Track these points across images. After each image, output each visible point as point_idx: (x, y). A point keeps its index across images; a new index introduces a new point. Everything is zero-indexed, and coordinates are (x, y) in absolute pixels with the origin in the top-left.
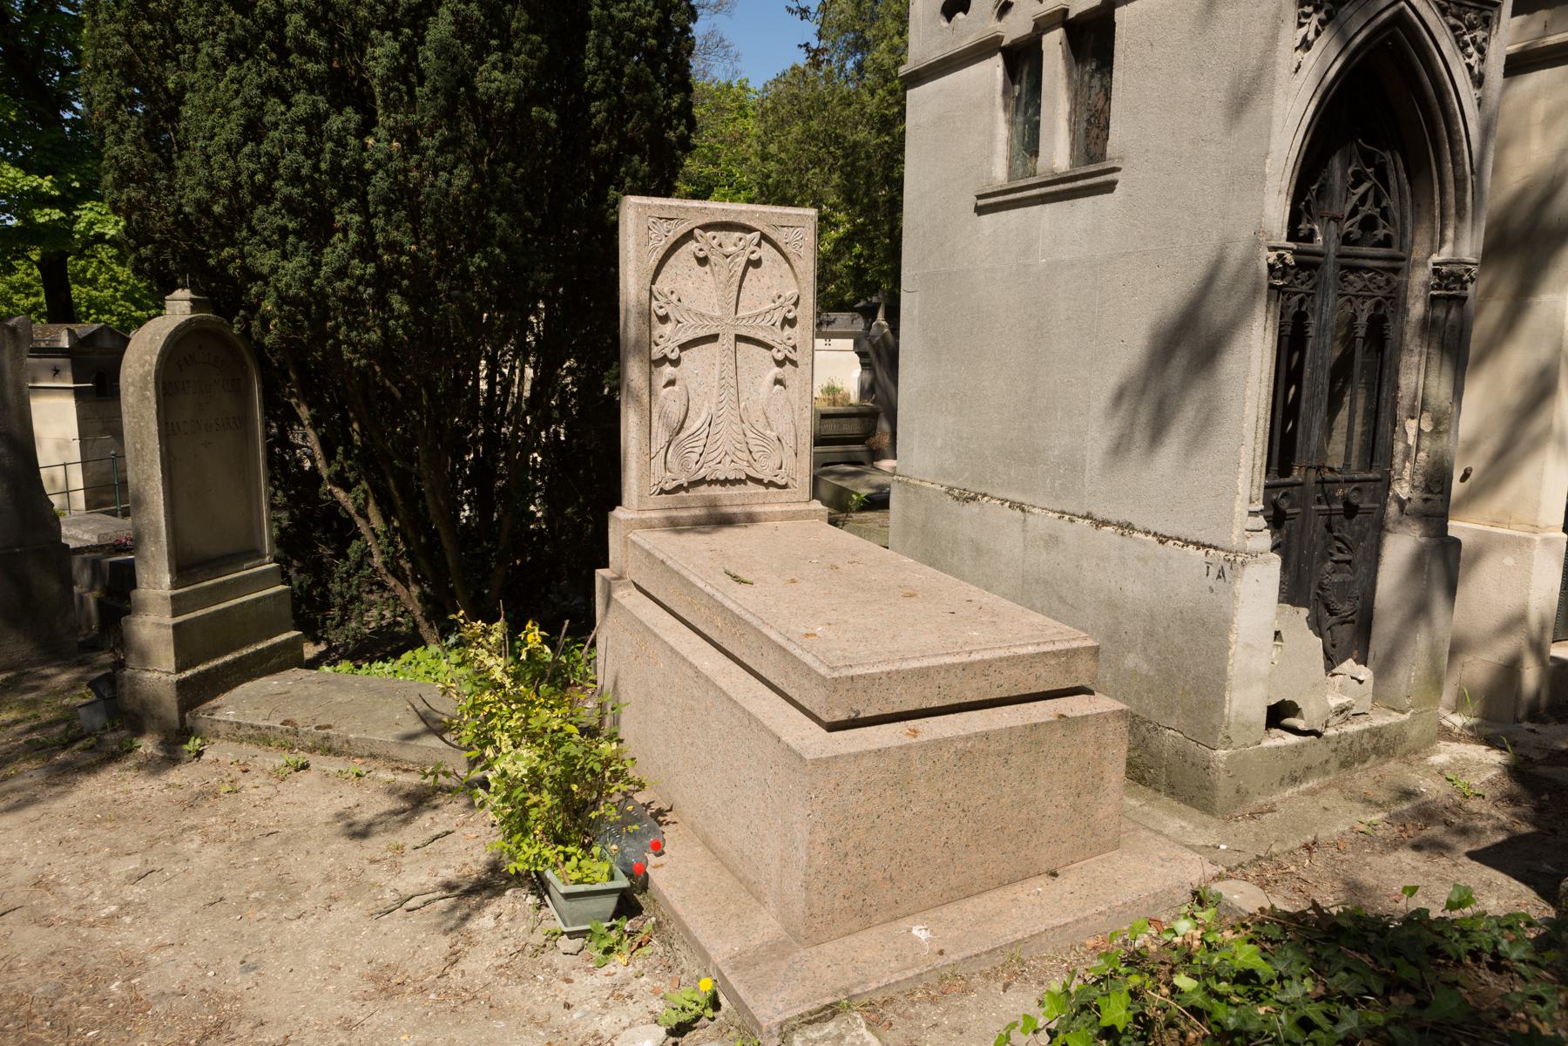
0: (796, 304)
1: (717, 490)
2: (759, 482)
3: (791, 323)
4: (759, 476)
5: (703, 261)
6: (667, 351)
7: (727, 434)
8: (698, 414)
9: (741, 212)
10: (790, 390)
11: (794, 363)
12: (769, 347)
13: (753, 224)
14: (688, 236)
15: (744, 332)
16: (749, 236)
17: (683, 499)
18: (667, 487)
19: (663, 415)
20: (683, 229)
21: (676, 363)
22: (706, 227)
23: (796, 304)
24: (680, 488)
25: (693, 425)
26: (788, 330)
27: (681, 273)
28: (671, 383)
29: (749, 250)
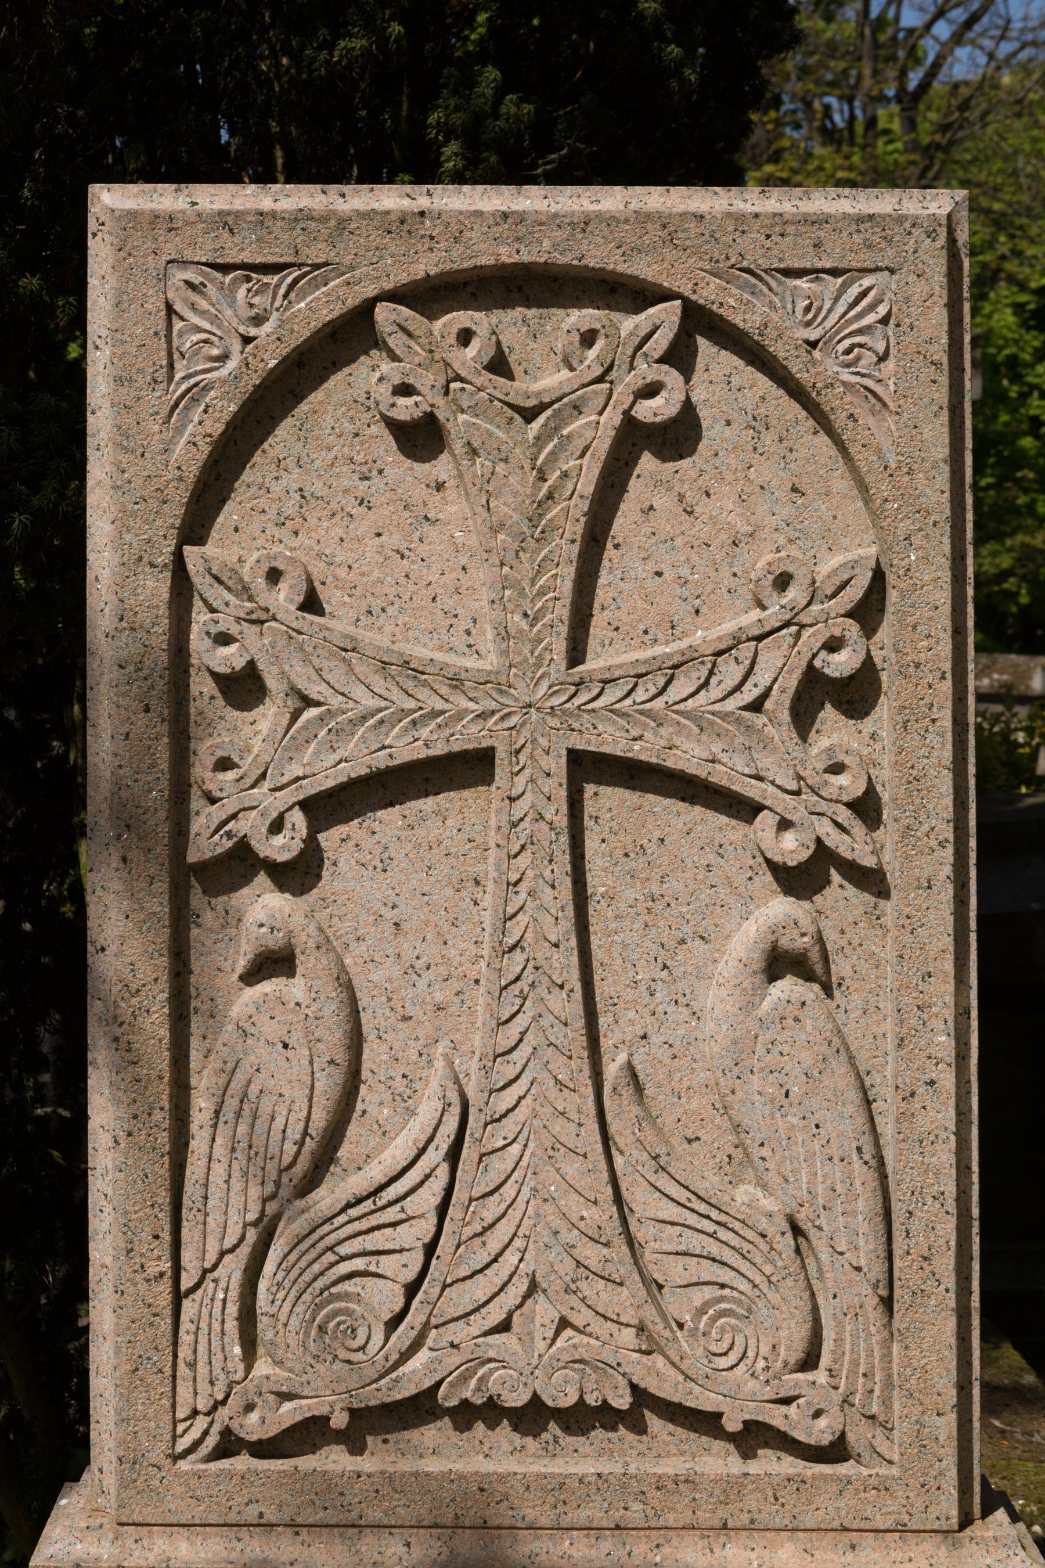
0: (869, 611)
1: (496, 1456)
2: (706, 1423)
3: (857, 695)
4: (705, 1400)
5: (420, 438)
6: (251, 826)
7: (541, 1194)
8: (405, 1104)
9: (585, 223)
10: (851, 1000)
11: (871, 880)
12: (745, 809)
13: (645, 269)
14: (350, 335)
15: (611, 740)
16: (630, 324)
17: (328, 1485)
18: (254, 1426)
19: (238, 1103)
20: (317, 307)
21: (300, 874)
22: (429, 296)
23: (869, 611)
24: (309, 1435)
25: (378, 1149)
26: (833, 729)
27: (327, 494)
28: (274, 963)
29: (627, 382)
